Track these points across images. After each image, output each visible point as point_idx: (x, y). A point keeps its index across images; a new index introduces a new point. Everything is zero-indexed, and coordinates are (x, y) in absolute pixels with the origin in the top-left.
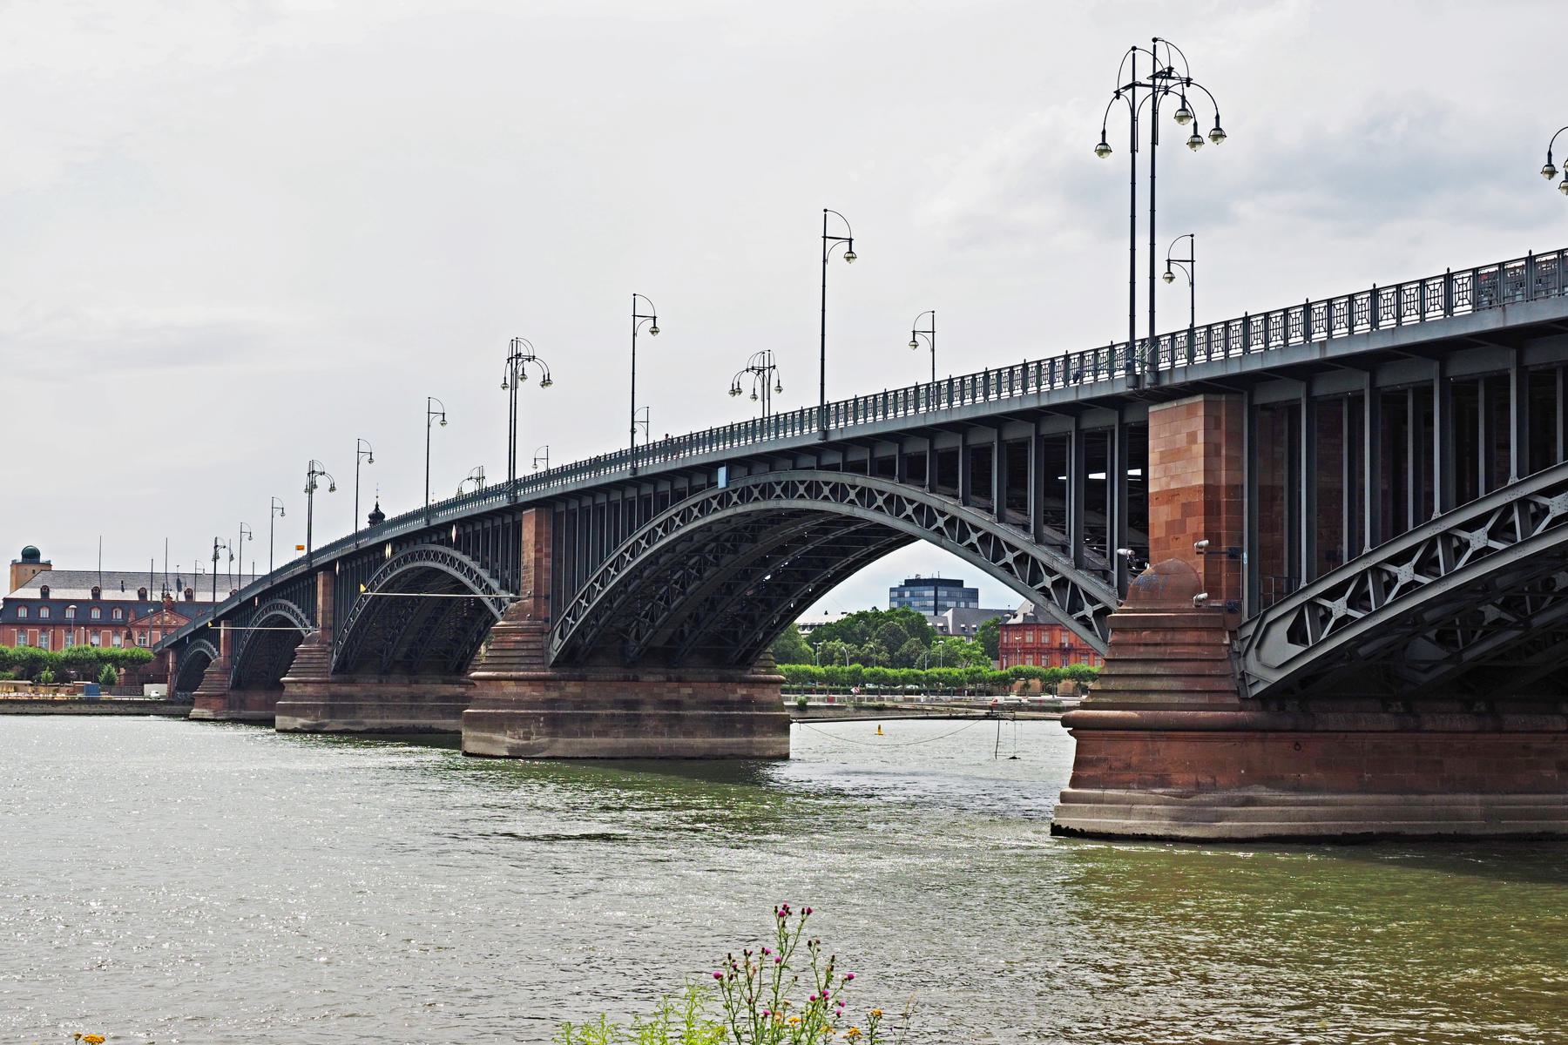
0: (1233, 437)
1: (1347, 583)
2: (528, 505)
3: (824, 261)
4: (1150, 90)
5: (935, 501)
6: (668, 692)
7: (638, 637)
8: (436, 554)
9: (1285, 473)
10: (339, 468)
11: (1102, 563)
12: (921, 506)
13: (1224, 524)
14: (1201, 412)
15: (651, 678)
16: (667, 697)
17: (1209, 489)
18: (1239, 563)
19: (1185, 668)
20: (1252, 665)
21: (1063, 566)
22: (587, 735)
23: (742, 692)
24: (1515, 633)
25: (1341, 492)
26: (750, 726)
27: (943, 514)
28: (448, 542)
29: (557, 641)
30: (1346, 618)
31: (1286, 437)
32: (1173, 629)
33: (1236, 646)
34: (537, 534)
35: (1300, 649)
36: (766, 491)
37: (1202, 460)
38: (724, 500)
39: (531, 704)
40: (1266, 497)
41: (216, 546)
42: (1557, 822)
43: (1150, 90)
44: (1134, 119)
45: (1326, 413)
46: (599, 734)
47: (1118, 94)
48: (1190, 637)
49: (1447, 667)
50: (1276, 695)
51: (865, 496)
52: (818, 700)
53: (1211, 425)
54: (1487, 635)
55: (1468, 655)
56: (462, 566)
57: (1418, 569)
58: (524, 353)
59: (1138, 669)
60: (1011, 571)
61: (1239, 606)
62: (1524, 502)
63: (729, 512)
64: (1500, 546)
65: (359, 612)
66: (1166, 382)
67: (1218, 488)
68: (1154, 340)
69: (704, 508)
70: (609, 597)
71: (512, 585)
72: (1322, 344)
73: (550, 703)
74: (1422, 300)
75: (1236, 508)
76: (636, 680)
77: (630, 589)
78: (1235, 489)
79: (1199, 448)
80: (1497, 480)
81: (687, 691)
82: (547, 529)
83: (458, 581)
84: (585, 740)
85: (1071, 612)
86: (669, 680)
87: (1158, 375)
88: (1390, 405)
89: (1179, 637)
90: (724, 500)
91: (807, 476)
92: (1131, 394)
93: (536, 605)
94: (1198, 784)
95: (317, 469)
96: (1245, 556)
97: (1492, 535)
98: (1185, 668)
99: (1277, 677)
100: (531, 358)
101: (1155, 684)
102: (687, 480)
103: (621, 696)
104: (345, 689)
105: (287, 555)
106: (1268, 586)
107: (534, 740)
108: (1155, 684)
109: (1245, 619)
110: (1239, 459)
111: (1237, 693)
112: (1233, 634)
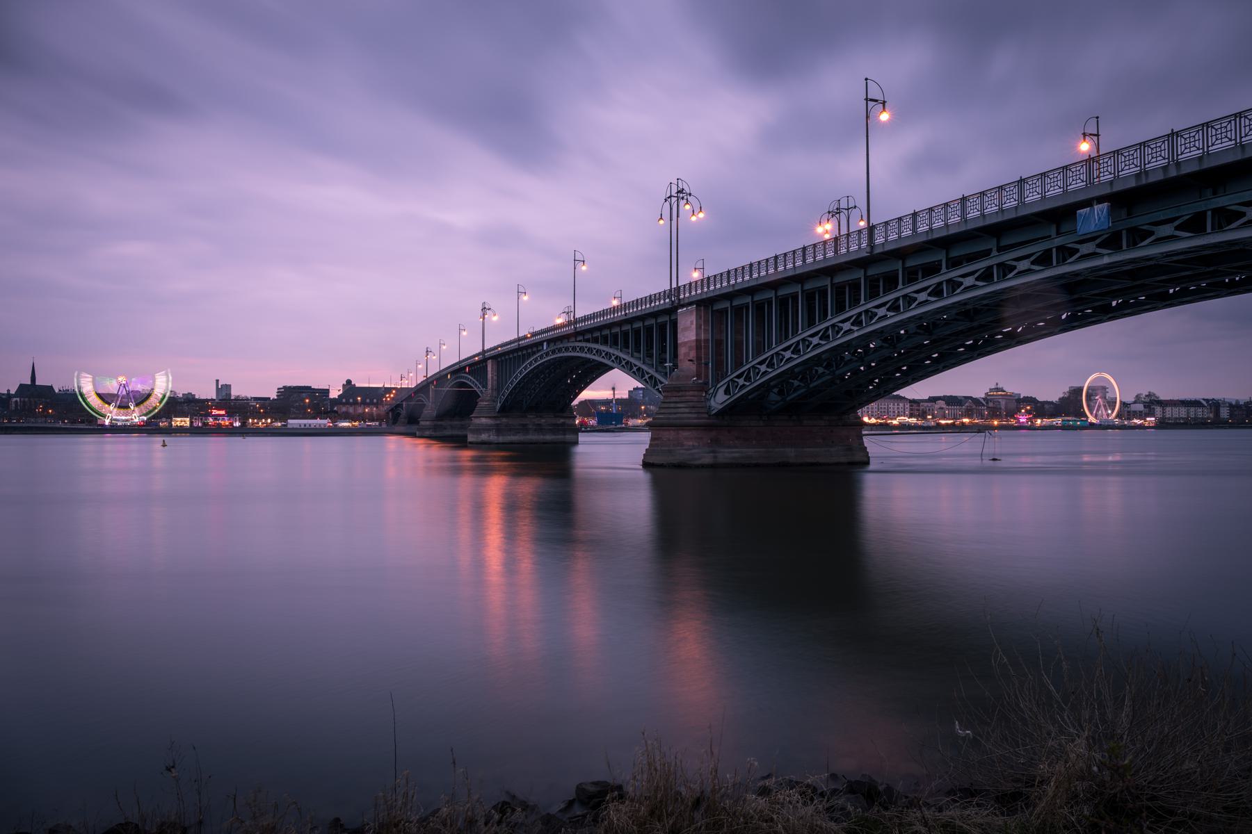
0: (706, 322)
1: (766, 359)
2: (489, 358)
3: (575, 268)
4: (676, 199)
5: (611, 351)
6: (537, 421)
7: (526, 402)
8: (464, 377)
9: (725, 334)
10: (434, 348)
11: (650, 363)
12: (617, 357)
13: (703, 353)
14: (695, 313)
15: (531, 416)
16: (537, 423)
17: (698, 341)
18: (708, 368)
19: (691, 404)
20: (712, 403)
21: (652, 372)
22: (510, 435)
23: (562, 420)
24: (804, 390)
25: (743, 341)
26: (564, 432)
27: (614, 355)
28: (465, 373)
29: (499, 404)
30: (744, 385)
31: (725, 323)
32: (686, 391)
33: (707, 396)
34: (492, 368)
35: (729, 397)
36: (560, 350)
37: (695, 330)
38: (547, 354)
39: (491, 425)
40: (719, 344)
41: (427, 351)
42: (808, 449)
43: (676, 199)
44: (671, 209)
45: (739, 311)
46: (513, 435)
47: (666, 200)
48: (691, 393)
49: (782, 403)
50: (722, 413)
51: (590, 350)
52: (452, 427)
53: (698, 317)
54: (795, 390)
55: (788, 399)
56: (471, 380)
57: (768, 366)
58: (487, 307)
59: (672, 405)
60: (635, 374)
61: (708, 382)
62: (833, 326)
63: (549, 358)
64: (795, 356)
65: (442, 397)
66: (682, 303)
67: (701, 340)
68: (679, 288)
69: (541, 357)
70: (515, 388)
71: (485, 386)
72: (733, 285)
73: (497, 425)
74: (767, 266)
75: (707, 347)
76: (526, 417)
77: (541, 386)
78: (706, 341)
79: (694, 326)
80: (795, 332)
81: (543, 421)
82: (495, 367)
83: (469, 385)
84: (509, 437)
85: (654, 387)
86: (537, 417)
87: (679, 300)
88: (759, 307)
89: (687, 393)
90: (547, 354)
91: (572, 345)
92: (671, 308)
93: (492, 392)
94: (693, 446)
95: (429, 350)
96: (710, 364)
97: (793, 353)
98: (691, 404)
99: (721, 407)
100: (489, 309)
101: (680, 410)
102: (774, 292)
103: (522, 423)
104: (439, 423)
105: (421, 379)
106: (718, 374)
107: (492, 437)
108: (680, 410)
109: (710, 387)
110: (708, 330)
111: (707, 413)
112: (706, 392)
